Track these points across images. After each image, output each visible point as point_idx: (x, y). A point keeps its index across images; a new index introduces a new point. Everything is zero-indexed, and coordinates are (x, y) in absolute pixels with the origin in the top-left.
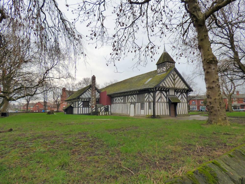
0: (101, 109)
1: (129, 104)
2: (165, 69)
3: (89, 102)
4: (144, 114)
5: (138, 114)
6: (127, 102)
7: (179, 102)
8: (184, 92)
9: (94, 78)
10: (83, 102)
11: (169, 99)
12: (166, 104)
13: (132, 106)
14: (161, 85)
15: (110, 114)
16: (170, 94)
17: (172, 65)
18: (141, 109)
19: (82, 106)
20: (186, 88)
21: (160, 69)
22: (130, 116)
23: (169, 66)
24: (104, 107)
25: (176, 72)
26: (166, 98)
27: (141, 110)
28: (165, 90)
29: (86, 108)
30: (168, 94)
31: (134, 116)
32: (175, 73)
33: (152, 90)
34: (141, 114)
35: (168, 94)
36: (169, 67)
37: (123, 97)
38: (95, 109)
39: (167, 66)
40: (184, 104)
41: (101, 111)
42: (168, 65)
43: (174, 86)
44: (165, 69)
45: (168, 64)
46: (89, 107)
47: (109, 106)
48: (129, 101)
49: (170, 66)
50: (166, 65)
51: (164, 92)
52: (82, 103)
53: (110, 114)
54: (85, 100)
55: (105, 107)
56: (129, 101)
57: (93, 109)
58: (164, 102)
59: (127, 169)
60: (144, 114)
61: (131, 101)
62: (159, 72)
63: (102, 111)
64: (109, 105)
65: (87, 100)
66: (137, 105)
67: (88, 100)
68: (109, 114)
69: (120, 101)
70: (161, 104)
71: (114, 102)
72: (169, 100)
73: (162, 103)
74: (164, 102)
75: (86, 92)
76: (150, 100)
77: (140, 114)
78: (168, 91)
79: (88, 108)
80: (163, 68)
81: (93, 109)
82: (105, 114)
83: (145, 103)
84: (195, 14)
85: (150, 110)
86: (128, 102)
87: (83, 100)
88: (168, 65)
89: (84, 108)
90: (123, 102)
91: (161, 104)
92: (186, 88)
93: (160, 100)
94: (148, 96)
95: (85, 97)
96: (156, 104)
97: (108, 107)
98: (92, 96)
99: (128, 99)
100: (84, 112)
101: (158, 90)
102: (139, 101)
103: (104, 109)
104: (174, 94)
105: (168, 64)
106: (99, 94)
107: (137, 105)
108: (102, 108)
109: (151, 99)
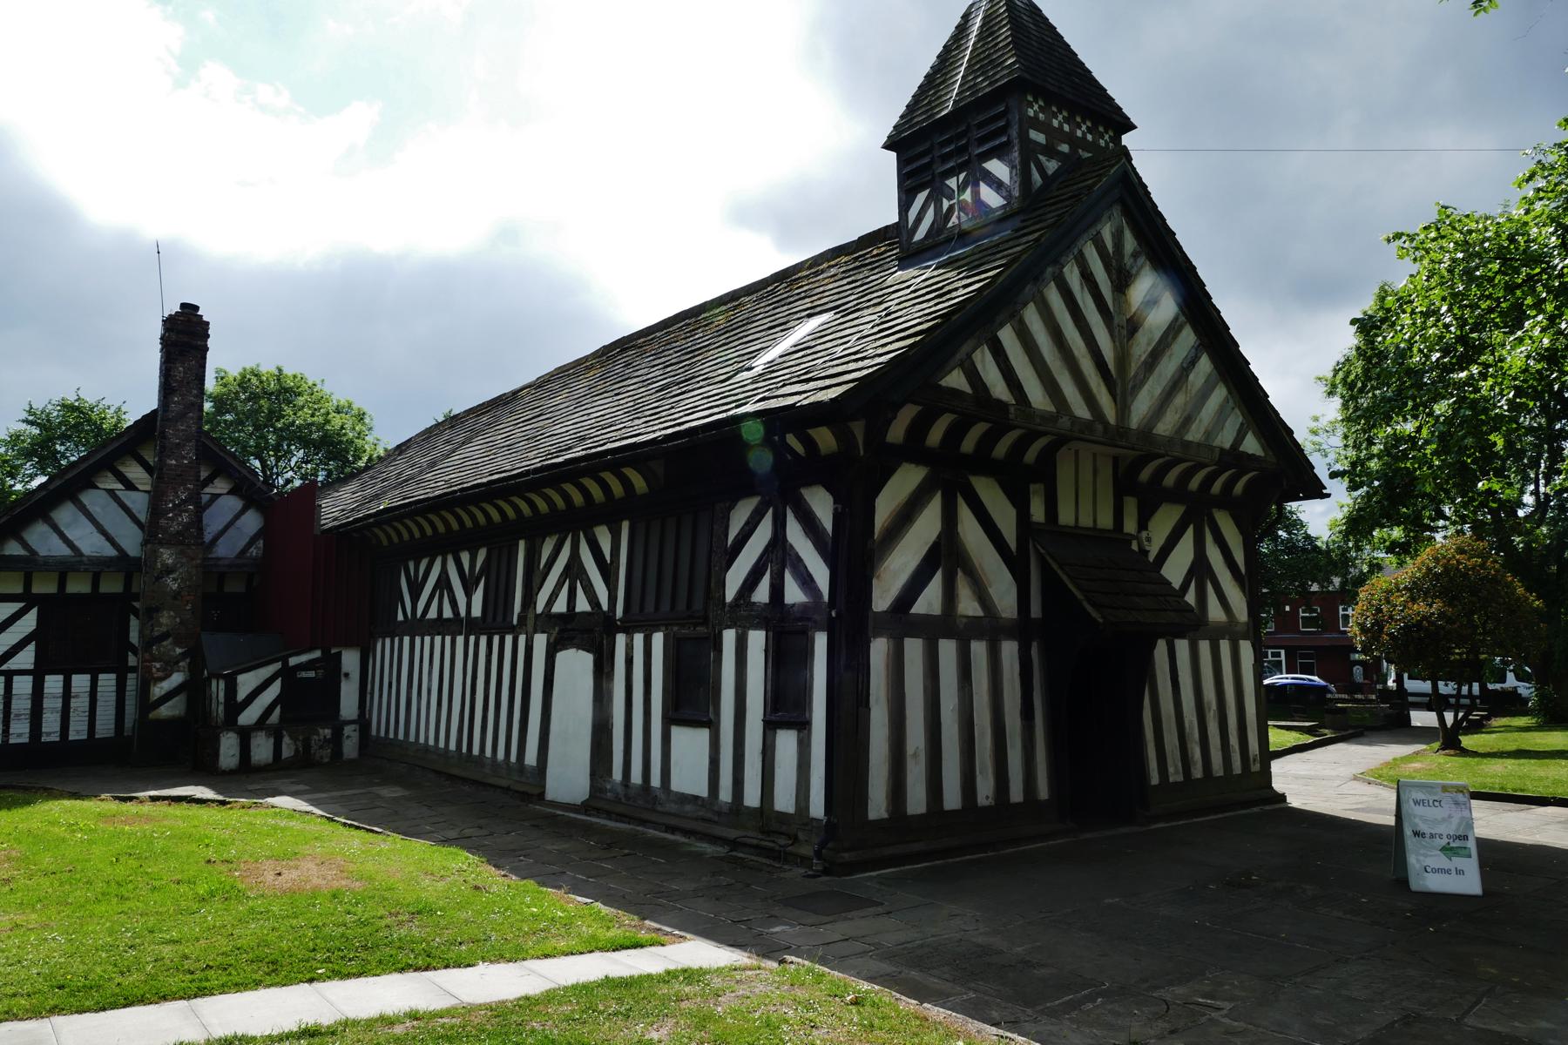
0: (231, 689)
1: (540, 641)
2: (997, 185)
3: (122, 605)
4: (702, 790)
5: (636, 777)
6: (522, 618)
7: (1172, 634)
8: (1225, 501)
9: (280, 370)
10: (40, 619)
11: (1045, 568)
12: (1009, 649)
13: (576, 665)
14: (956, 380)
15: (350, 747)
16: (1066, 516)
17: (1092, 146)
18: (669, 720)
19: (26, 658)
20: (1251, 445)
21: (936, 197)
22: (542, 794)
23: (1050, 151)
24: (277, 666)
25: (1138, 235)
26: (1016, 563)
27: (677, 733)
28: (1001, 449)
29: (438, 639)
30: (1038, 512)
31: (586, 807)
32: (1130, 244)
33: (825, 438)
34: (679, 784)
35: (1038, 512)
36: (1052, 166)
37: (482, 555)
38: (31, 647)
39: (1029, 153)
40: (1225, 646)
41: (230, 721)
42: (1038, 137)
43: (1123, 409)
44: (997, 185)
45: (1035, 124)
46: (122, 674)
47: (350, 660)
48: (540, 608)
49: (1065, 148)
50: (1014, 132)
51: (990, 493)
52: (29, 622)
53: (350, 747)
54: (78, 586)
55: (287, 674)
56: (540, 608)
57: (159, 690)
58: (990, 628)
59: (705, 926)
60: (702, 790)
61: (560, 606)
62: (920, 234)
63: (249, 716)
64: (349, 644)
65: (227, 589)
66: (629, 661)
67: (111, 585)
68: (337, 752)
69: (983, 597)
70: (948, 649)
71: (400, 617)
72: (1052, 588)
73: (965, 632)
74: (990, 628)
75: (89, 498)
76: (794, 594)
77: (656, 781)
78: (1045, 472)
79: (107, 681)
80: (972, 182)
81: (159, 690)
82: (287, 751)
83: (729, 637)
84: (716, 808)
85: (786, 742)
86: (531, 616)
87: (45, 586)
88: (1038, 137)
89: (53, 683)
90: (477, 611)
91: (948, 649)
92: (1251, 445)
93: (929, 601)
94: (927, 526)
95: (65, 551)
96: (879, 649)
97: (332, 672)
98: (152, 530)
99: (537, 580)
100: (57, 727)
101: (913, 450)
102: (650, 607)
103: (274, 690)
104: (1106, 521)
105: (1035, 124)
106: (252, 522)
107: (629, 661)
108: (247, 682)
109: (806, 581)
